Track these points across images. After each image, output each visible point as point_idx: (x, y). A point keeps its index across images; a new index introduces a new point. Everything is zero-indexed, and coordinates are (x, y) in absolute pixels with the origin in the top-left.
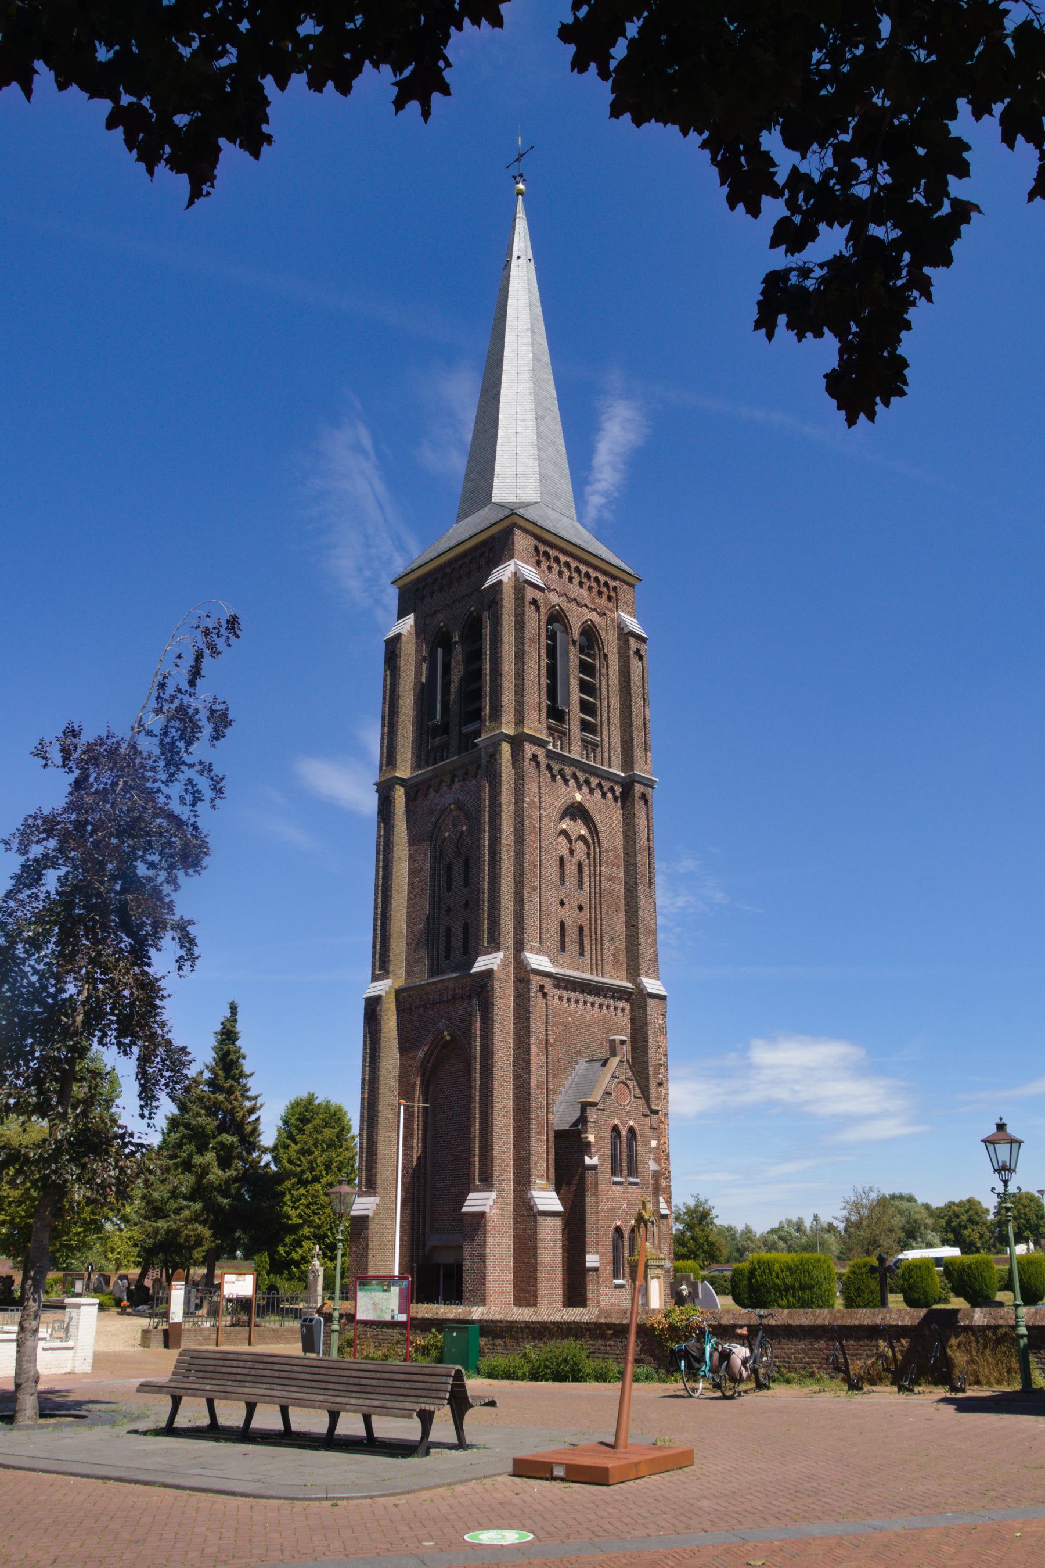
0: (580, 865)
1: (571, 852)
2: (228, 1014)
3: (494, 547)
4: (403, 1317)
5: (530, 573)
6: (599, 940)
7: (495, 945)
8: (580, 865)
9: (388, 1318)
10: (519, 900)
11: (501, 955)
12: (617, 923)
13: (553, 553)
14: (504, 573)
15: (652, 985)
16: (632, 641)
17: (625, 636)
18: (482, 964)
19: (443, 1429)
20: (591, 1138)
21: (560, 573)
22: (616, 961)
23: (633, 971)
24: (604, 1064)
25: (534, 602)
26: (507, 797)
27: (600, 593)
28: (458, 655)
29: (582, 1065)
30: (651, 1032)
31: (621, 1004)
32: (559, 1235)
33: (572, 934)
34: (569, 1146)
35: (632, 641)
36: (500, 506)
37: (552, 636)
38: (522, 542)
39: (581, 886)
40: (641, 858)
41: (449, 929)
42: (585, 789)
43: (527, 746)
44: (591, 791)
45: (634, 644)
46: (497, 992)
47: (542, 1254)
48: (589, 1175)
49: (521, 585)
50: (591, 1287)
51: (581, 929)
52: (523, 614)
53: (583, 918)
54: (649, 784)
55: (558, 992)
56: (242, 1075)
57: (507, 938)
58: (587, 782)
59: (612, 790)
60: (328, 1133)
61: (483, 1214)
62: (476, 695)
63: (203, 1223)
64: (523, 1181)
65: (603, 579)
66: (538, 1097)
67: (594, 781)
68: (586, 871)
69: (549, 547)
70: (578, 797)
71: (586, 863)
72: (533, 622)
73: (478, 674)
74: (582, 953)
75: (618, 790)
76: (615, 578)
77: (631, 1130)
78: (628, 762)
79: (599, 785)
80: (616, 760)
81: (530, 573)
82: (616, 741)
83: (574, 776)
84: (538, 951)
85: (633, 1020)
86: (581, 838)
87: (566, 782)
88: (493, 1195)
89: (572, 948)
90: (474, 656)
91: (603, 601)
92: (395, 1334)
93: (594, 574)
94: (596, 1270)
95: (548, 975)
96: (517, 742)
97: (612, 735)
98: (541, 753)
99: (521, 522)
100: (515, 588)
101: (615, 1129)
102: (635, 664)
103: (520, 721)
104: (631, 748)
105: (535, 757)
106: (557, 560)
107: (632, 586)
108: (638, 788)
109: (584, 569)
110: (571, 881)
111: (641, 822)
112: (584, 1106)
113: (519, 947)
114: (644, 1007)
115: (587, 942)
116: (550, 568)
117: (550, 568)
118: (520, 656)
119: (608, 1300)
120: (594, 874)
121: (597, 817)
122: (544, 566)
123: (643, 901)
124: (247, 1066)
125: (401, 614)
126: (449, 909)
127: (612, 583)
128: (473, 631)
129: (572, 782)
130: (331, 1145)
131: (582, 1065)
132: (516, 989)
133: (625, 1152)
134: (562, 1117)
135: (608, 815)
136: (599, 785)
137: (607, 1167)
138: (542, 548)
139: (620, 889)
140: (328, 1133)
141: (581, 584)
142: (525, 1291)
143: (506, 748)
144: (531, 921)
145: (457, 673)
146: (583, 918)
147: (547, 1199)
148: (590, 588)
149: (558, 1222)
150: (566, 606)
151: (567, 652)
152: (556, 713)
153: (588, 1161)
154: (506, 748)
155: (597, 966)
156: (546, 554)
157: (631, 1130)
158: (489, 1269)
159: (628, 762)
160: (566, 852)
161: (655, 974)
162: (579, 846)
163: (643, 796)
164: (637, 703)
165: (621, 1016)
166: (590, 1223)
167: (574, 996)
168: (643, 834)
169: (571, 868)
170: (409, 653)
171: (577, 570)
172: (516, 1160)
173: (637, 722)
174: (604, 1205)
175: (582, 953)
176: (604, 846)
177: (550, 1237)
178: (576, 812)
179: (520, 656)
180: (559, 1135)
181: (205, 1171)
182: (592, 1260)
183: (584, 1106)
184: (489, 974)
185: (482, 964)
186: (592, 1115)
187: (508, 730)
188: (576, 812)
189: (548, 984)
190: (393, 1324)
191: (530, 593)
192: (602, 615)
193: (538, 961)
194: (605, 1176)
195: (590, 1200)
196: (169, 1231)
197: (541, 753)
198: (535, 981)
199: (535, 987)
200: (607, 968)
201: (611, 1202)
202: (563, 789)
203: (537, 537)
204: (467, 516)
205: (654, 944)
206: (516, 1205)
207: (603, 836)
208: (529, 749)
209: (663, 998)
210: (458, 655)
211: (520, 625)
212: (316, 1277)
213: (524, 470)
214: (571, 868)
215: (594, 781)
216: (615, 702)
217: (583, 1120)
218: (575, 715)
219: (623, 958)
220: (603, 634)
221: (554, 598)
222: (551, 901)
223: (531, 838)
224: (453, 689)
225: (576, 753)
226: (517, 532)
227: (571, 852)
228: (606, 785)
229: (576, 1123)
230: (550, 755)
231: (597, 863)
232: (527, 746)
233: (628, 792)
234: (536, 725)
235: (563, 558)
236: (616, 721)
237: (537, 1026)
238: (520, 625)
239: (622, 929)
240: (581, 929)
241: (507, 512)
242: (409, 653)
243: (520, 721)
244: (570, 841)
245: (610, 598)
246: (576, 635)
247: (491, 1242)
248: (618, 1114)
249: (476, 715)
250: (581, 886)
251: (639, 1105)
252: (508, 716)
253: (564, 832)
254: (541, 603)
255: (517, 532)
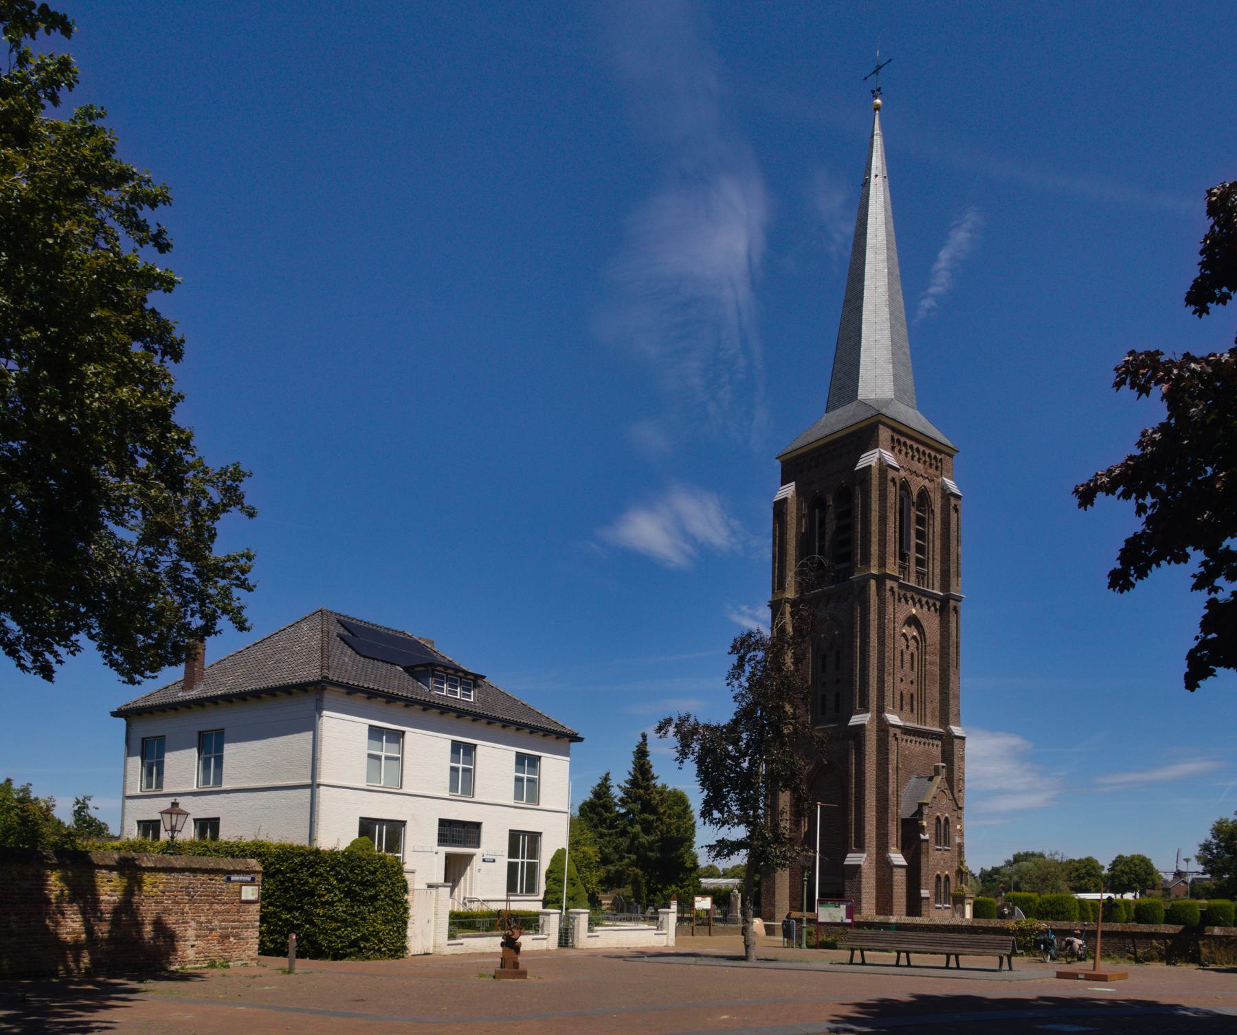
0: (912, 655)
1: (908, 647)
2: (641, 740)
3: (863, 435)
4: (849, 921)
5: (890, 458)
6: (923, 702)
7: (865, 709)
8: (912, 655)
9: (839, 921)
10: (881, 681)
11: (869, 715)
12: (934, 692)
13: (902, 439)
14: (869, 459)
15: (956, 730)
16: (952, 499)
17: (947, 495)
18: (855, 720)
19: (1005, 966)
20: (925, 824)
21: (907, 454)
22: (933, 716)
23: (944, 720)
24: (931, 779)
25: (893, 480)
26: (873, 616)
27: (931, 465)
28: (831, 515)
29: (914, 780)
30: (956, 760)
31: (936, 742)
32: (904, 879)
33: (907, 699)
34: (911, 828)
35: (952, 499)
36: (864, 404)
37: (902, 500)
38: (884, 434)
39: (912, 669)
40: (952, 650)
41: (824, 697)
42: (918, 606)
43: (888, 582)
44: (922, 607)
45: (953, 501)
46: (867, 737)
47: (895, 889)
48: (924, 845)
49: (884, 467)
50: (924, 908)
51: (912, 695)
52: (885, 490)
53: (913, 689)
54: (959, 599)
55: (905, 737)
56: (653, 778)
57: (873, 705)
58: (920, 601)
59: (934, 605)
60: (677, 809)
61: (859, 866)
62: (849, 542)
63: (637, 866)
64: (882, 848)
65: (933, 454)
66: (892, 799)
67: (924, 600)
68: (916, 659)
69: (903, 436)
70: (914, 611)
71: (916, 653)
72: (892, 493)
73: (849, 528)
74: (912, 711)
75: (938, 604)
76: (940, 452)
77: (946, 819)
78: (945, 585)
79: (927, 603)
80: (937, 584)
81: (890, 458)
82: (937, 571)
83: (912, 598)
84: (892, 713)
85: (943, 752)
86: (914, 637)
87: (907, 602)
88: (865, 855)
89: (907, 708)
90: (846, 515)
91: (932, 471)
92: (840, 929)
93: (927, 451)
94: (927, 898)
95: (899, 727)
96: (881, 579)
97: (936, 568)
98: (895, 585)
99: (884, 419)
100: (880, 470)
101: (938, 818)
102: (953, 515)
103: (882, 564)
104: (949, 576)
105: (892, 588)
106: (905, 444)
107: (951, 456)
108: (952, 603)
109: (922, 448)
110: (907, 666)
111: (953, 625)
112: (921, 805)
113: (881, 710)
114: (952, 744)
115: (915, 704)
116: (900, 451)
117: (900, 451)
118: (883, 520)
119: (938, 914)
120: (921, 661)
121: (924, 624)
122: (896, 450)
123: (952, 677)
124: (655, 771)
125: (784, 482)
126: (824, 683)
127: (939, 457)
128: (845, 496)
129: (910, 602)
130: (679, 817)
131: (914, 780)
132: (878, 735)
133: (944, 831)
134: (907, 811)
135: (931, 622)
136: (927, 603)
137: (933, 841)
138: (896, 437)
139: (936, 670)
140: (677, 809)
141: (919, 460)
142: (884, 905)
143: (873, 582)
144: (888, 694)
145: (830, 528)
146: (913, 689)
147: (898, 858)
148: (925, 462)
149: (904, 871)
150: (909, 477)
151: (909, 511)
152: (903, 556)
153: (922, 836)
154: (873, 582)
155: (922, 718)
156: (898, 441)
157: (946, 819)
158: (863, 896)
159: (945, 585)
160: (904, 647)
161: (958, 724)
162: (912, 643)
163: (955, 609)
164: (953, 542)
165: (936, 749)
166: (923, 872)
167: (909, 738)
168: (954, 634)
169: (907, 657)
170: (792, 510)
171: (918, 450)
172: (877, 835)
173: (953, 557)
174: (932, 862)
175: (912, 711)
176: (928, 642)
177: (900, 878)
178: (913, 621)
179: (883, 520)
180: (904, 821)
181: (636, 837)
182: (924, 893)
183: (921, 805)
184: (862, 727)
185: (855, 720)
186: (926, 810)
187: (874, 571)
188: (913, 621)
189: (898, 731)
190: (842, 924)
191: (891, 474)
192: (932, 481)
193: (893, 719)
194: (932, 845)
195: (923, 859)
196: (616, 871)
197: (895, 585)
198: (892, 730)
199: (891, 734)
200: (928, 720)
201: (936, 861)
202: (905, 607)
203: (894, 430)
204: (835, 408)
205: (958, 705)
206: (877, 861)
207: (927, 635)
208: (889, 583)
209: (963, 738)
210: (831, 515)
211: (883, 497)
212: (736, 899)
213: (879, 376)
214: (907, 657)
215: (924, 600)
216: (938, 544)
217: (919, 813)
218: (913, 554)
219: (937, 713)
220: (932, 495)
221: (902, 473)
222: (900, 680)
223: (889, 642)
224: (828, 538)
225: (912, 583)
226: (881, 426)
227: (908, 647)
228: (931, 602)
229: (915, 814)
230: (901, 586)
231: (922, 652)
232: (888, 582)
233: (945, 606)
234: (892, 568)
235: (909, 442)
236: (938, 557)
237: (893, 757)
238: (883, 497)
239: (937, 695)
240: (912, 695)
241: (874, 413)
242: (792, 510)
243: (882, 564)
244: (907, 640)
245: (937, 468)
246: (915, 498)
247: (864, 881)
248: (939, 810)
249: (848, 557)
250: (912, 669)
251: (951, 805)
252: (874, 562)
253: (904, 635)
254: (897, 481)
255: (881, 426)
